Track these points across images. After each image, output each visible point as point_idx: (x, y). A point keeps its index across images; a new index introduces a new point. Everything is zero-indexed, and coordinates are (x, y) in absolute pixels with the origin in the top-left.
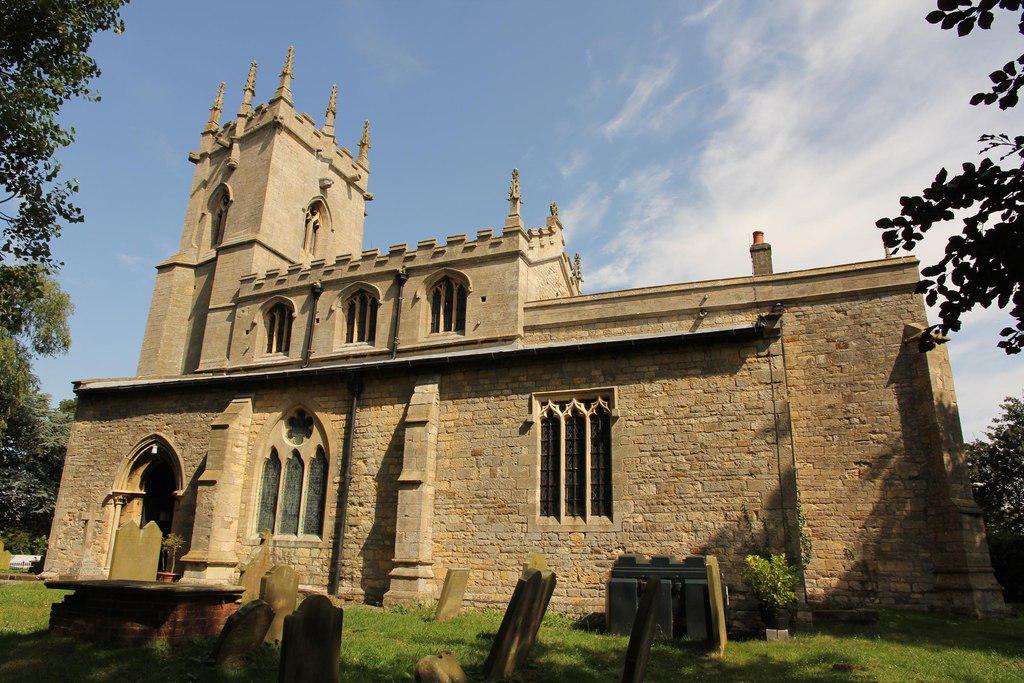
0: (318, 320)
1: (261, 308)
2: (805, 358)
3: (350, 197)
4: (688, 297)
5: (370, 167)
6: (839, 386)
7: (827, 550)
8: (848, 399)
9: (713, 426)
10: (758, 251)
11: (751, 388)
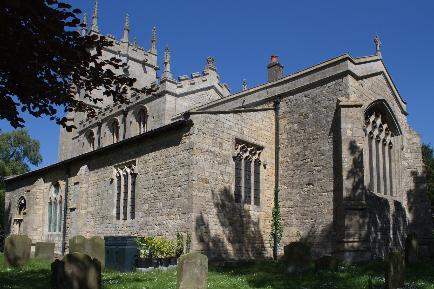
0: (101, 138)
1: (85, 136)
2: (288, 127)
3: (145, 72)
4: (236, 101)
5: (157, 52)
6: (303, 141)
7: (289, 232)
8: (306, 148)
9: (167, 174)
10: (271, 67)
11: (182, 153)
